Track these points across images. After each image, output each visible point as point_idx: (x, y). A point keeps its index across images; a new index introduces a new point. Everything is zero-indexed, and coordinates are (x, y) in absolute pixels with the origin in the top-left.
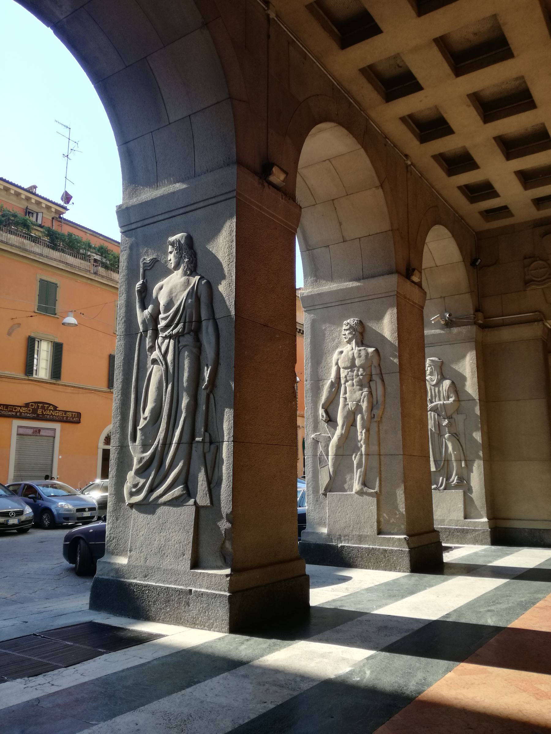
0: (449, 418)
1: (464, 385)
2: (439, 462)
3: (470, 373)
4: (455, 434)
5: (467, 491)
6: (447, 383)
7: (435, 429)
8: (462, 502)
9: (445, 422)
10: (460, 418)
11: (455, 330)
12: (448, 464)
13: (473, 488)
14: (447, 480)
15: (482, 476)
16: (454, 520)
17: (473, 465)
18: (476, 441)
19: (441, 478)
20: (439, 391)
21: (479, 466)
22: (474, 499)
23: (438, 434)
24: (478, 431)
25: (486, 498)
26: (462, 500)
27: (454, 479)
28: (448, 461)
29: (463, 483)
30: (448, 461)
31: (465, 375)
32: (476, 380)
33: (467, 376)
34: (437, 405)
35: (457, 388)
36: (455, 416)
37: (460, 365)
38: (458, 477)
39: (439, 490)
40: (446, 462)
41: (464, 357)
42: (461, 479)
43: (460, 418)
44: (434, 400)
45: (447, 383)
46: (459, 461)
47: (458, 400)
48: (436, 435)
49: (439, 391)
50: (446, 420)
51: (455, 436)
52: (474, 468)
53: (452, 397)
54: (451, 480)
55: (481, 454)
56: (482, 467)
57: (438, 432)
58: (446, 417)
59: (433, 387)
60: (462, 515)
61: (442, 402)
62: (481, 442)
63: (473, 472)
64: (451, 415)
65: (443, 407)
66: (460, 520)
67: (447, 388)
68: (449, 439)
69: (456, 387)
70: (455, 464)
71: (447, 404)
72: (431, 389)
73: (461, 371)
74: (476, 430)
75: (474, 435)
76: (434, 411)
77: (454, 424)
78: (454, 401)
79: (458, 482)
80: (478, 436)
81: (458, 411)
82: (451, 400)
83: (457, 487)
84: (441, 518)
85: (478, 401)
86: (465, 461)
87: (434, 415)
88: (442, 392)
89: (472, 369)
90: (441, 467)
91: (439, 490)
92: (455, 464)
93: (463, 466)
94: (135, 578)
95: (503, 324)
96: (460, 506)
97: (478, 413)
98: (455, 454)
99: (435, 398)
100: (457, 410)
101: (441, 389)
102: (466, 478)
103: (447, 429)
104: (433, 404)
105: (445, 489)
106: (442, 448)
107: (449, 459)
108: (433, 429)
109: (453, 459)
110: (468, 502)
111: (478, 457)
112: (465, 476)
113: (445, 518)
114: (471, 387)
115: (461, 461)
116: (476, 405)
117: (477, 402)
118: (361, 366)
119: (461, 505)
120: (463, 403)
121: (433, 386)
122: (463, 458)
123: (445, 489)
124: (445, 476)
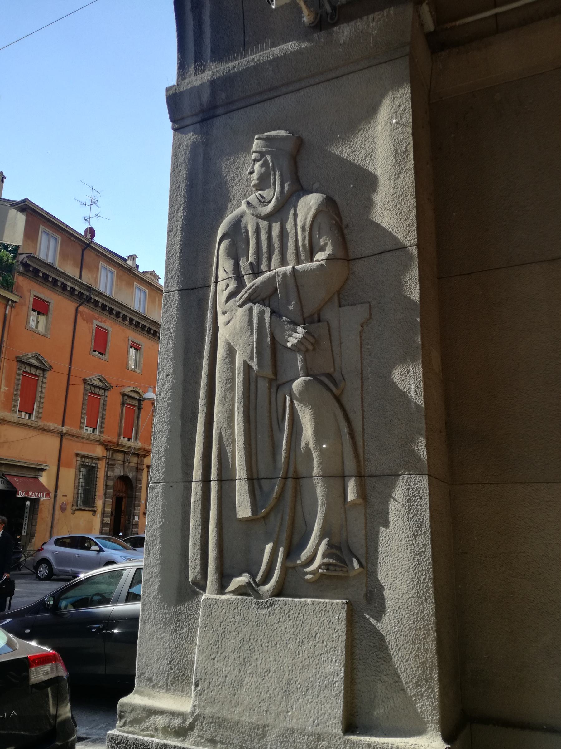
0: (312, 320)
1: (369, 204)
2: (265, 484)
3: (391, 160)
4: (329, 376)
5: (365, 602)
6: (309, 204)
7: (259, 364)
8: (341, 656)
9: (295, 336)
10: (347, 322)
11: (345, 32)
12: (297, 492)
13: (387, 593)
14: (288, 555)
15: (425, 539)
16: (303, 733)
17: (389, 496)
18: (404, 396)
19: (269, 547)
20: (283, 234)
21: (411, 500)
22: (390, 640)
23: (271, 381)
24: (414, 360)
25: (439, 641)
26: (341, 644)
27: (316, 552)
28: (297, 478)
29: (350, 572)
30: (296, 479)
31: (371, 169)
32: (408, 178)
33: (379, 172)
34: (273, 278)
35: (344, 217)
36: (330, 314)
37: (358, 140)
38: (329, 545)
39: (258, 596)
40: (290, 483)
41: (372, 111)
42: (340, 552)
43: (347, 322)
44: (264, 267)
45: (309, 204)
46: (336, 479)
47: (344, 256)
48: (263, 385)
49: (283, 234)
50: (300, 329)
51: (328, 384)
52: (393, 506)
53: (322, 249)
54: (305, 554)
55: (421, 449)
56: (426, 501)
57: (269, 372)
58: (299, 319)
59: (264, 224)
60: (334, 711)
61: (289, 268)
62: (420, 401)
63: (386, 525)
64: (319, 312)
65: (291, 282)
66: (330, 737)
67: (309, 219)
68: (306, 397)
69: (339, 215)
70: (320, 491)
71: (305, 272)
72: (258, 231)
73: (358, 158)
74: (403, 360)
75: (397, 375)
76: (262, 302)
77: (325, 343)
78: (329, 259)
79: (327, 566)
80: (409, 380)
81: (341, 296)
82: (321, 256)
83: (324, 585)
84: (254, 719)
85: (414, 251)
86: (360, 477)
87: (261, 314)
88: (291, 233)
89: (397, 144)
90: (271, 502)
91: (258, 596)
92: (320, 491)
93: (351, 497)
94: (337, 604)
95: (499, 28)
96: (329, 668)
97: (414, 292)
98: (322, 453)
99: (269, 259)
100: (339, 293)
101: (289, 225)
102: (361, 551)
103: (299, 358)
104: (261, 279)
105: (279, 592)
106: (281, 431)
107: (302, 470)
108: (254, 364)
109: (316, 471)
110: (363, 650)
111: (412, 465)
112: (358, 542)
113: (270, 721)
114: (393, 209)
115: (343, 477)
116: (406, 268)
117: (411, 257)
118: (174, 332)
119: (335, 667)
120: (359, 267)
121: (265, 218)
122: (350, 465)
123: (279, 592)
124: (284, 537)
